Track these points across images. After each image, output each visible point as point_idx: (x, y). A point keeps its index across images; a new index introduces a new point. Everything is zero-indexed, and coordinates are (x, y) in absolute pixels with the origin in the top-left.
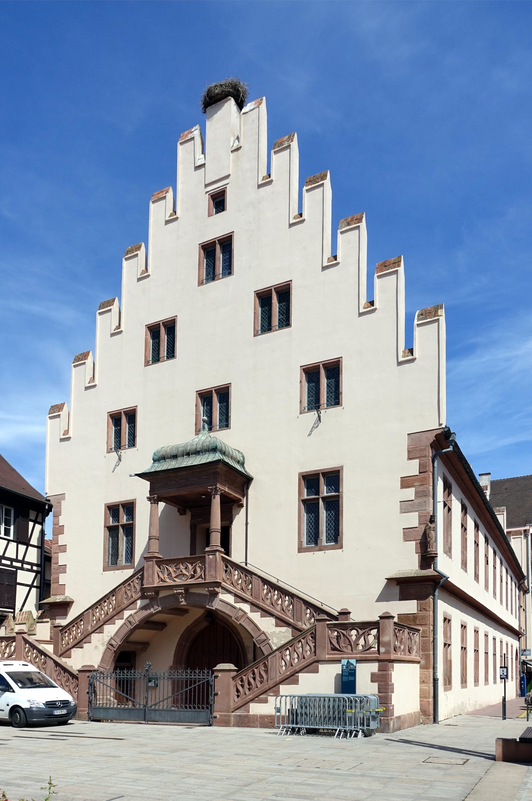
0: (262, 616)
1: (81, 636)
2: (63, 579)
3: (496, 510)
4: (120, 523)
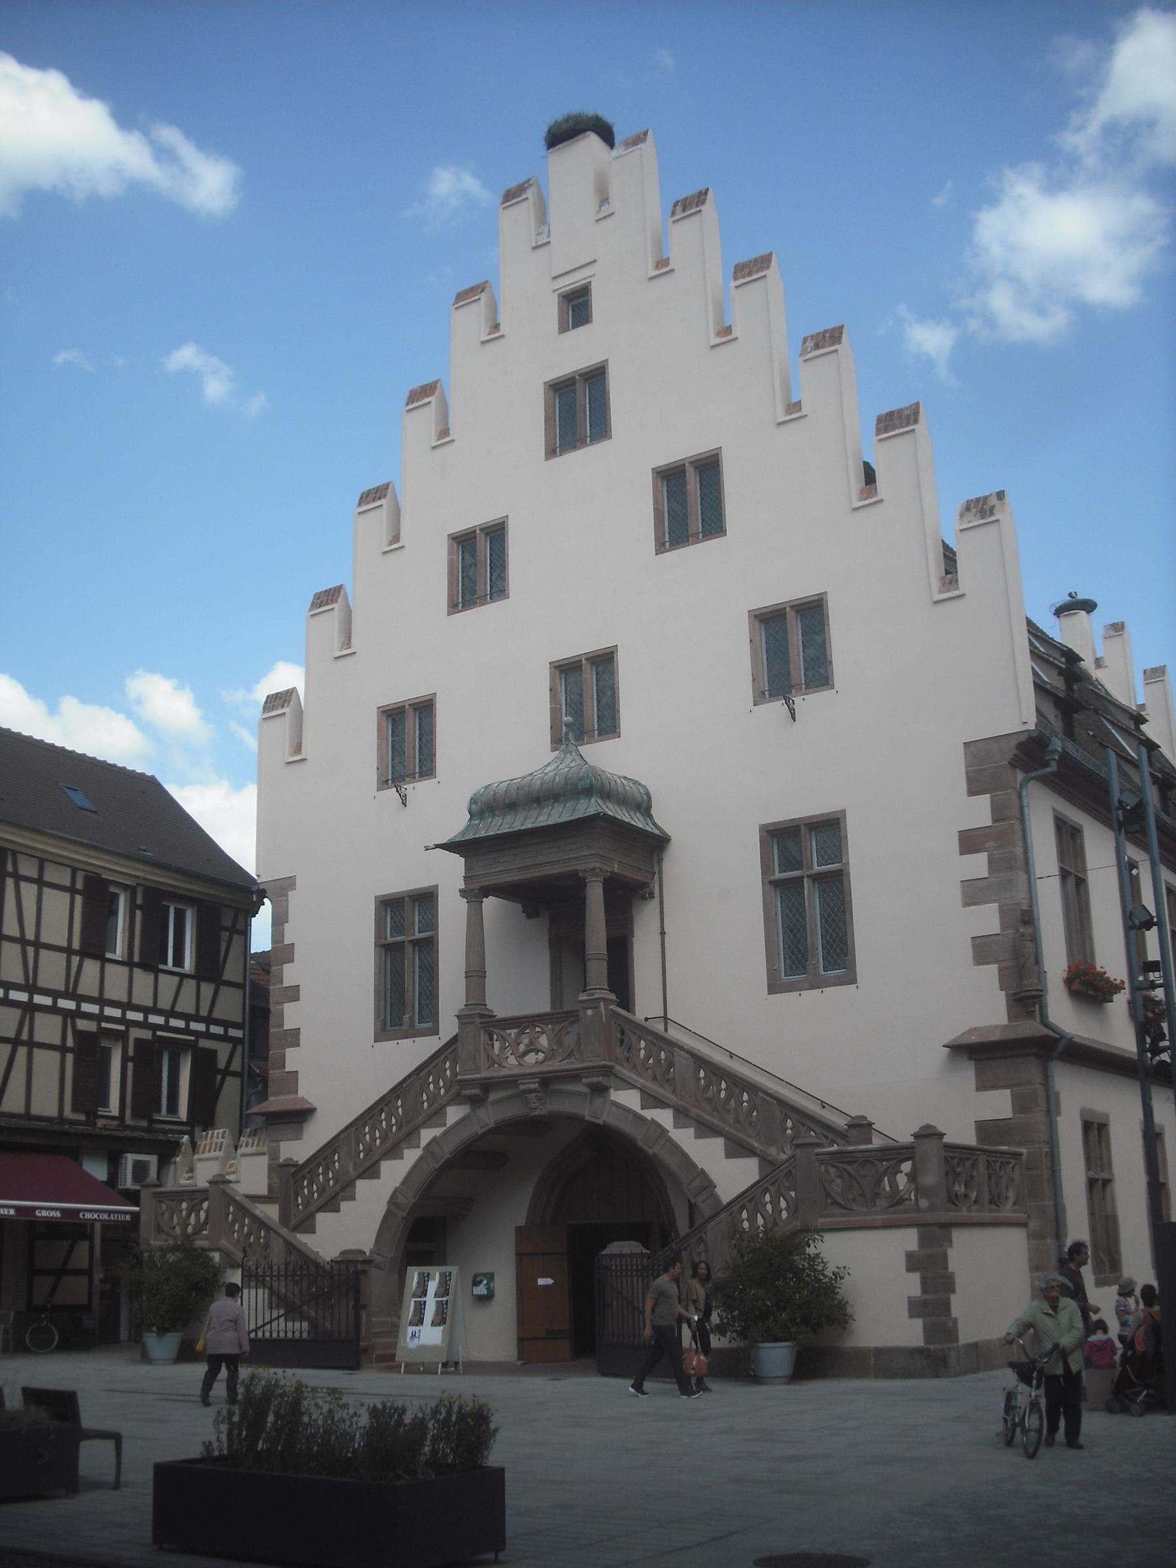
0: (697, 1136)
2: (293, 1059)
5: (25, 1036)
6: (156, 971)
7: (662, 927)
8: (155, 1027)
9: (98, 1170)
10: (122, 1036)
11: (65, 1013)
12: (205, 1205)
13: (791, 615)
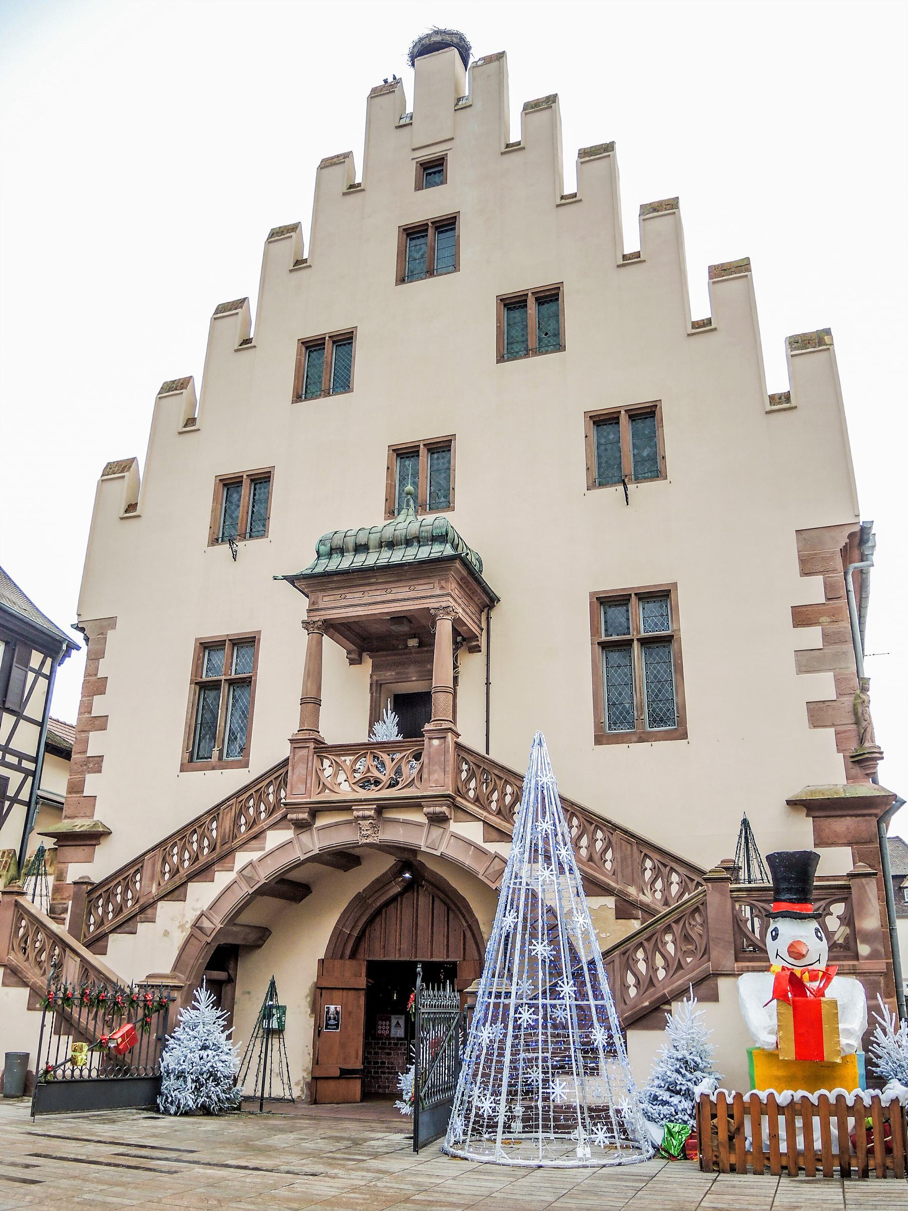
1: (133, 906)
4: (223, 678)
7: (488, 679)
13: (624, 419)
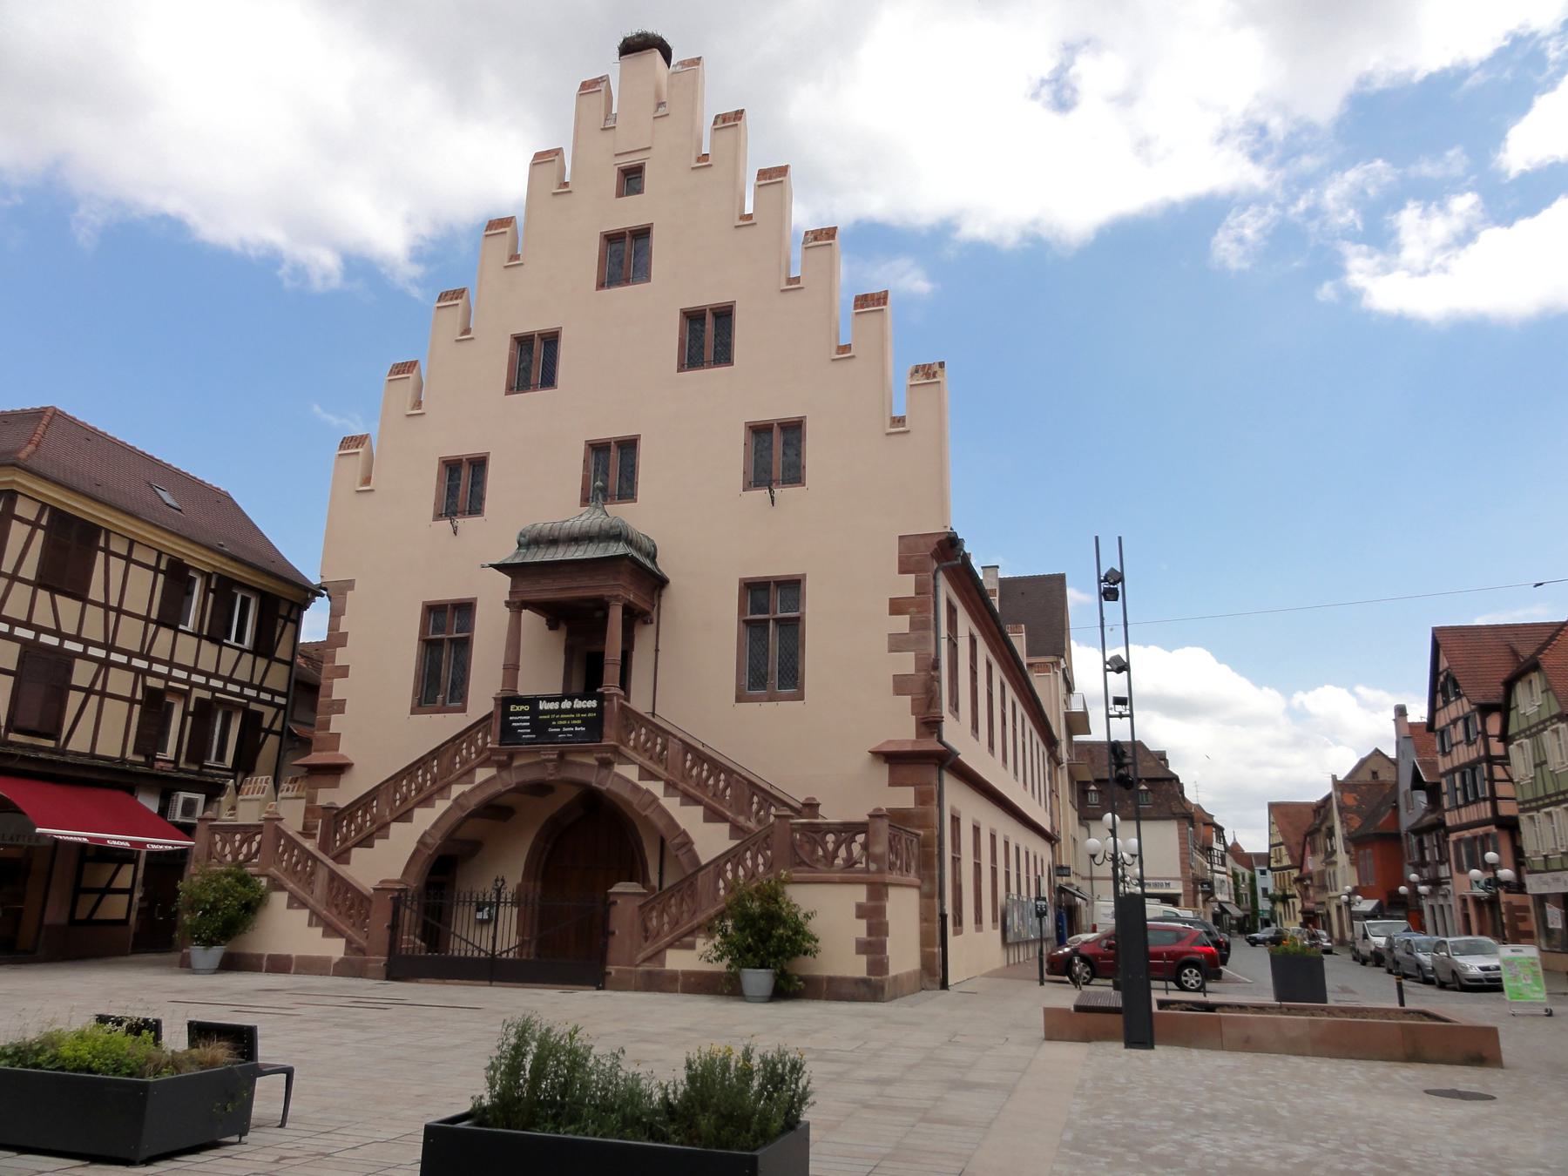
2: (337, 723)
3: (1008, 628)
5: (98, 687)
6: (221, 644)
8: (214, 690)
9: (151, 804)
10: (185, 695)
11: (138, 671)
12: (258, 838)
13: (776, 430)
